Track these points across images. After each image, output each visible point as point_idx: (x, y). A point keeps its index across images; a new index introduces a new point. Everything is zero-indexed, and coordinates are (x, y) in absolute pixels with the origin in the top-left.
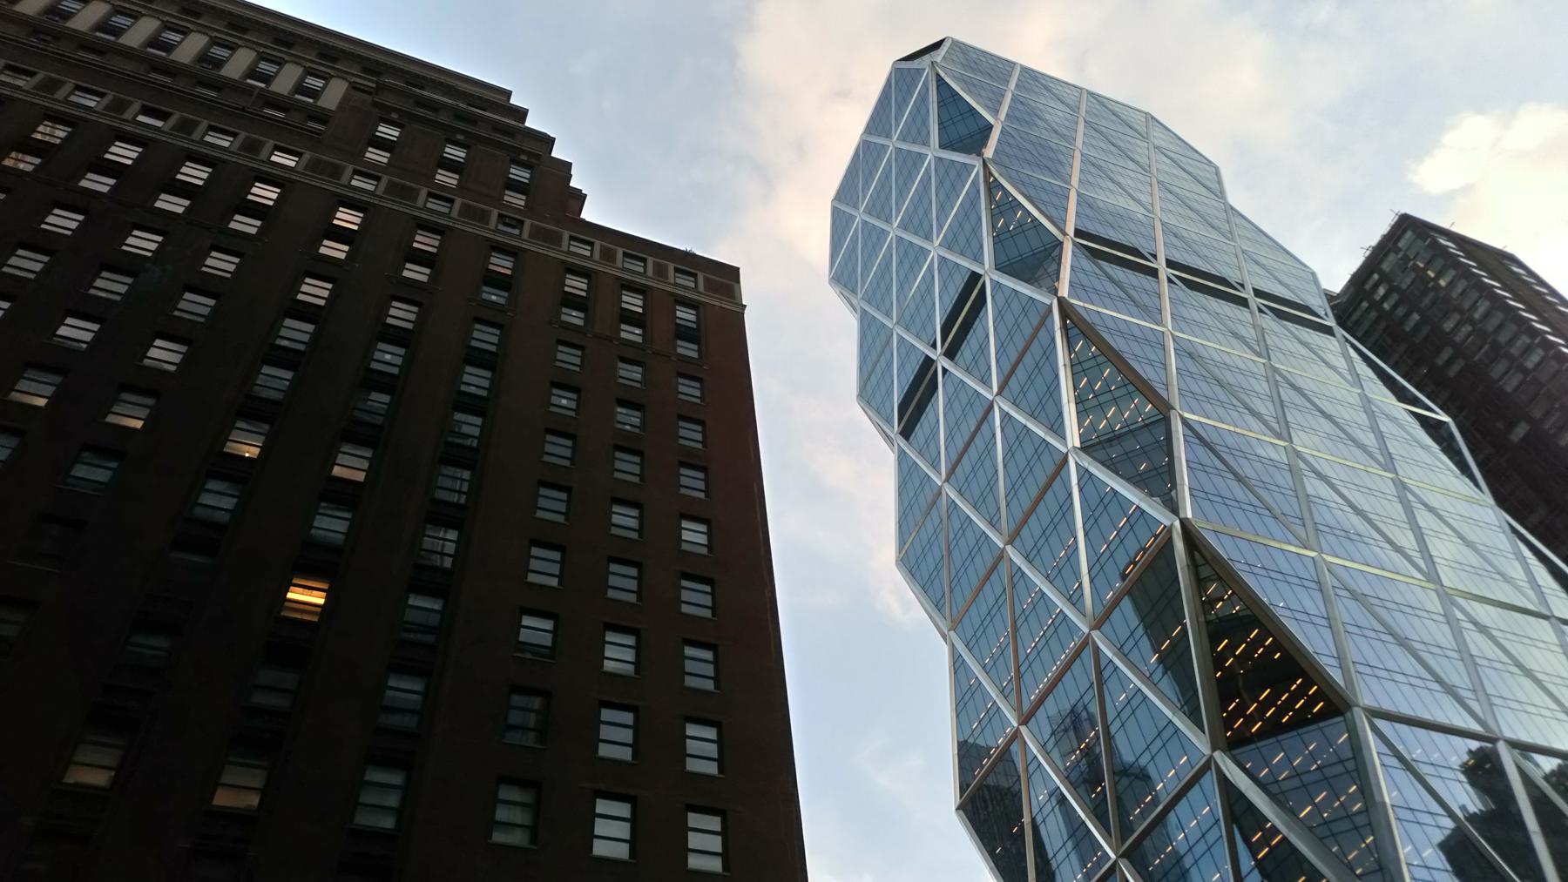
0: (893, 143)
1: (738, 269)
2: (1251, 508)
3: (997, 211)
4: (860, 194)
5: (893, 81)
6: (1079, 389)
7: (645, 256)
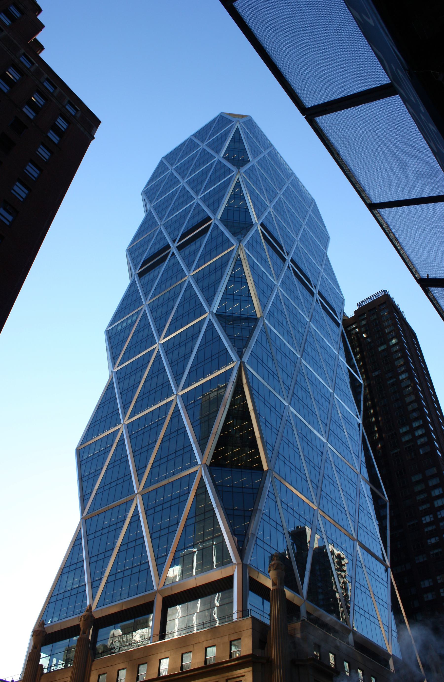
0: (203, 146)
1: (100, 122)
2: (272, 373)
3: (233, 196)
4: (177, 160)
5: (217, 120)
6: (228, 288)
7: (57, 86)
